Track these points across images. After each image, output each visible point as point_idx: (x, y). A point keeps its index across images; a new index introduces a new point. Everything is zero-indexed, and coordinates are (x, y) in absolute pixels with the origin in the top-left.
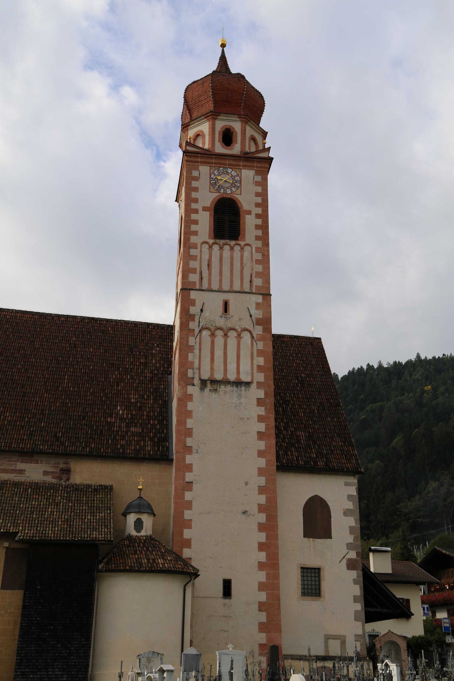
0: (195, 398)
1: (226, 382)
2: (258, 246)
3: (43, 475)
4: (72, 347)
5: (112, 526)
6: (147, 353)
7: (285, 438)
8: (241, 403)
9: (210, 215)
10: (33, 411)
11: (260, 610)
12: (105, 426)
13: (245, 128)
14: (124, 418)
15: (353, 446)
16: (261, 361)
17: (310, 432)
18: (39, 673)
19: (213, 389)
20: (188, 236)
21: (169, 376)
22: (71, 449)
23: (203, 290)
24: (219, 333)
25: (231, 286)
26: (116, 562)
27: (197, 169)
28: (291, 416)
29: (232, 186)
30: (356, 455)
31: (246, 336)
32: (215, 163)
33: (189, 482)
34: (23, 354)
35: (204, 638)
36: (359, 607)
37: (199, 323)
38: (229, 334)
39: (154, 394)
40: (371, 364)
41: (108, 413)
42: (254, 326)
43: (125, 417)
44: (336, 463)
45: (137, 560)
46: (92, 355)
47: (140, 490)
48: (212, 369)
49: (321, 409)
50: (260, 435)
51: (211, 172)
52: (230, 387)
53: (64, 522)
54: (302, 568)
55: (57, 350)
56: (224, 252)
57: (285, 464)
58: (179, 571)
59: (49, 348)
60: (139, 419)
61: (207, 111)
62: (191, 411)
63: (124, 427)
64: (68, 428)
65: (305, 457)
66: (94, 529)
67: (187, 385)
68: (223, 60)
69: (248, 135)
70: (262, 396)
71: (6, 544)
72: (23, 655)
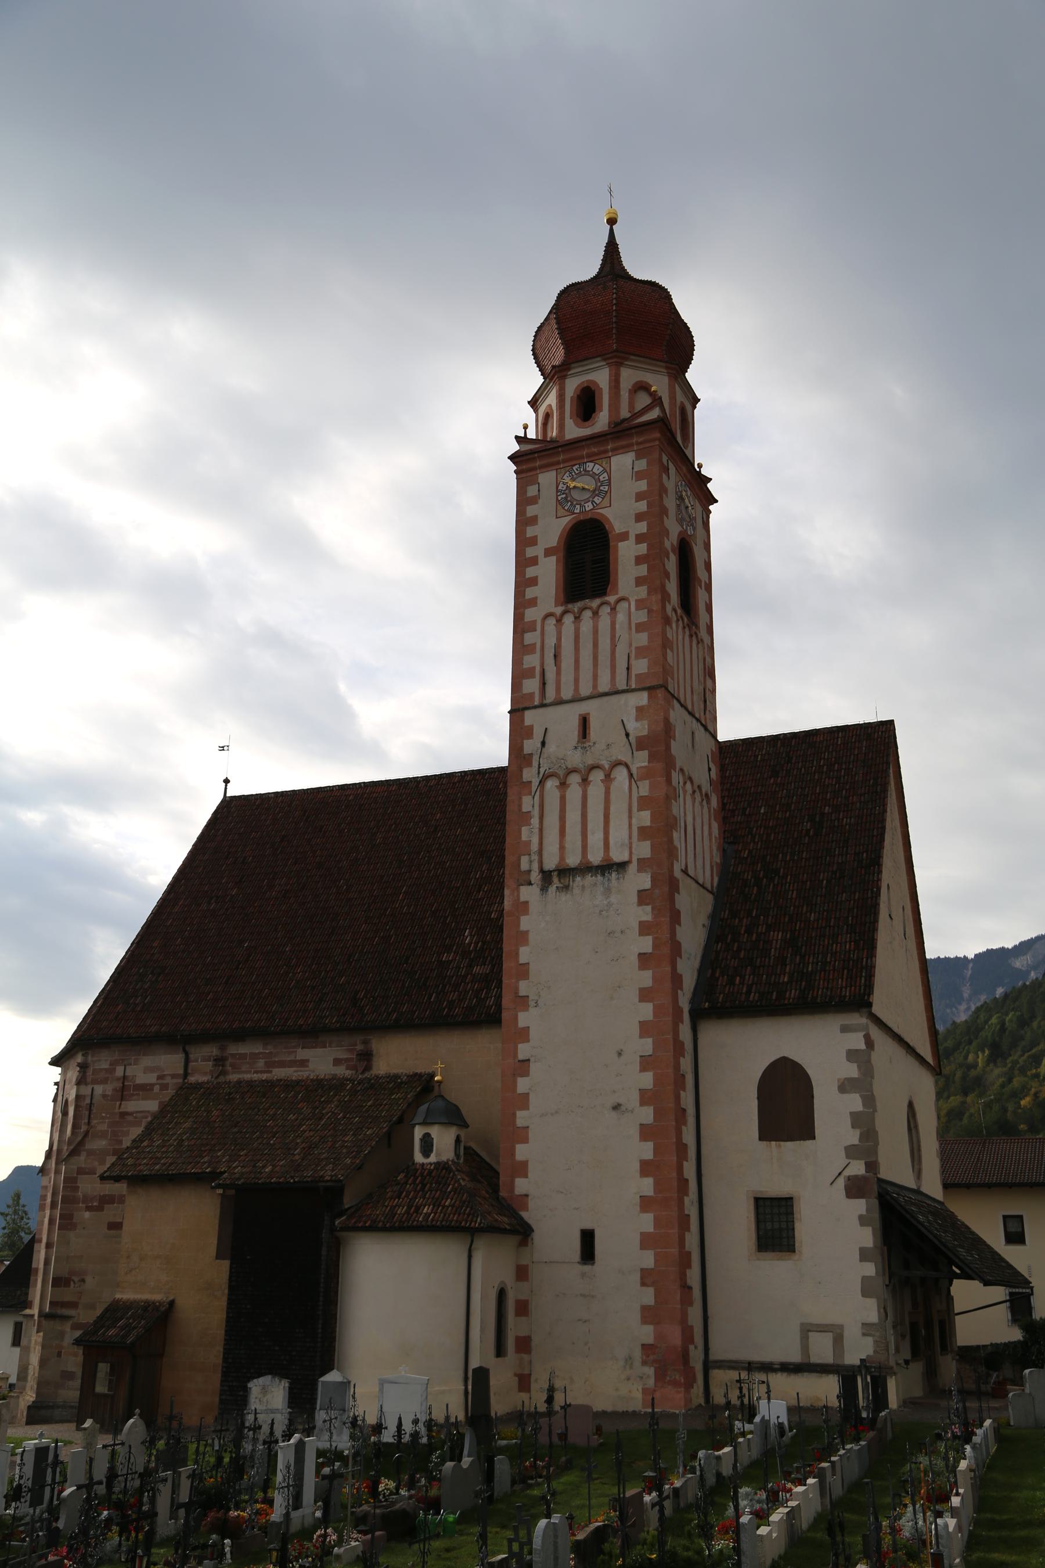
0: (532, 908)
1: (586, 869)
2: (640, 597)
3: (334, 1065)
9: (558, 561)
11: (643, 1284)
19: (562, 885)
24: (574, 779)
25: (595, 686)
31: (621, 776)
32: (564, 461)
33: (523, 1061)
37: (539, 767)
38: (591, 778)
42: (633, 753)
48: (562, 848)
52: (592, 876)
56: (582, 624)
62: (527, 932)
67: (520, 885)
68: (612, 249)
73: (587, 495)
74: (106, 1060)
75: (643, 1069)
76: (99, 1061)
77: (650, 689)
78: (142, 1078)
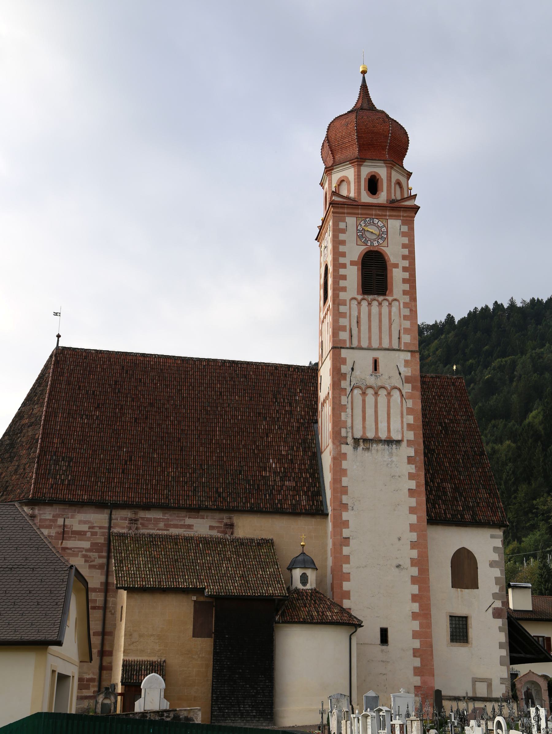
0: (348, 457)
1: (377, 441)
2: (405, 301)
4: (218, 395)
5: (283, 581)
6: (291, 399)
7: (432, 490)
8: (392, 462)
10: (192, 466)
11: (414, 656)
12: (261, 480)
13: (391, 174)
14: (277, 472)
15: (499, 498)
16: (410, 419)
17: (456, 484)
18: (232, 709)
20: (337, 292)
21: (315, 425)
22: (233, 505)
23: (353, 348)
24: (370, 392)
25: (380, 343)
26: (290, 614)
27: (344, 221)
28: (437, 466)
29: (378, 238)
30: (501, 508)
31: (396, 394)
32: (361, 214)
34: (173, 405)
35: (365, 681)
36: (504, 652)
37: (351, 382)
38: (379, 393)
39: (303, 446)
40: (499, 303)
41: (262, 467)
43: (278, 471)
44: (482, 516)
45: (309, 612)
46: (238, 404)
47: (303, 546)
48: (364, 427)
49: (465, 459)
50: (411, 492)
51: (358, 224)
52: (382, 445)
53: (240, 577)
54: (450, 616)
55: (204, 398)
57: (434, 518)
58: (346, 623)
59: (197, 397)
60: (292, 473)
61: (353, 157)
62: (346, 470)
63: (278, 481)
64: (227, 483)
65: (452, 510)
66: (268, 585)
69: (393, 181)
70: (413, 454)
71: (194, 598)
72: (218, 693)
73: (375, 237)
74: (50, 514)
75: (412, 548)
76: (45, 514)
77: (412, 352)
78: (77, 527)
